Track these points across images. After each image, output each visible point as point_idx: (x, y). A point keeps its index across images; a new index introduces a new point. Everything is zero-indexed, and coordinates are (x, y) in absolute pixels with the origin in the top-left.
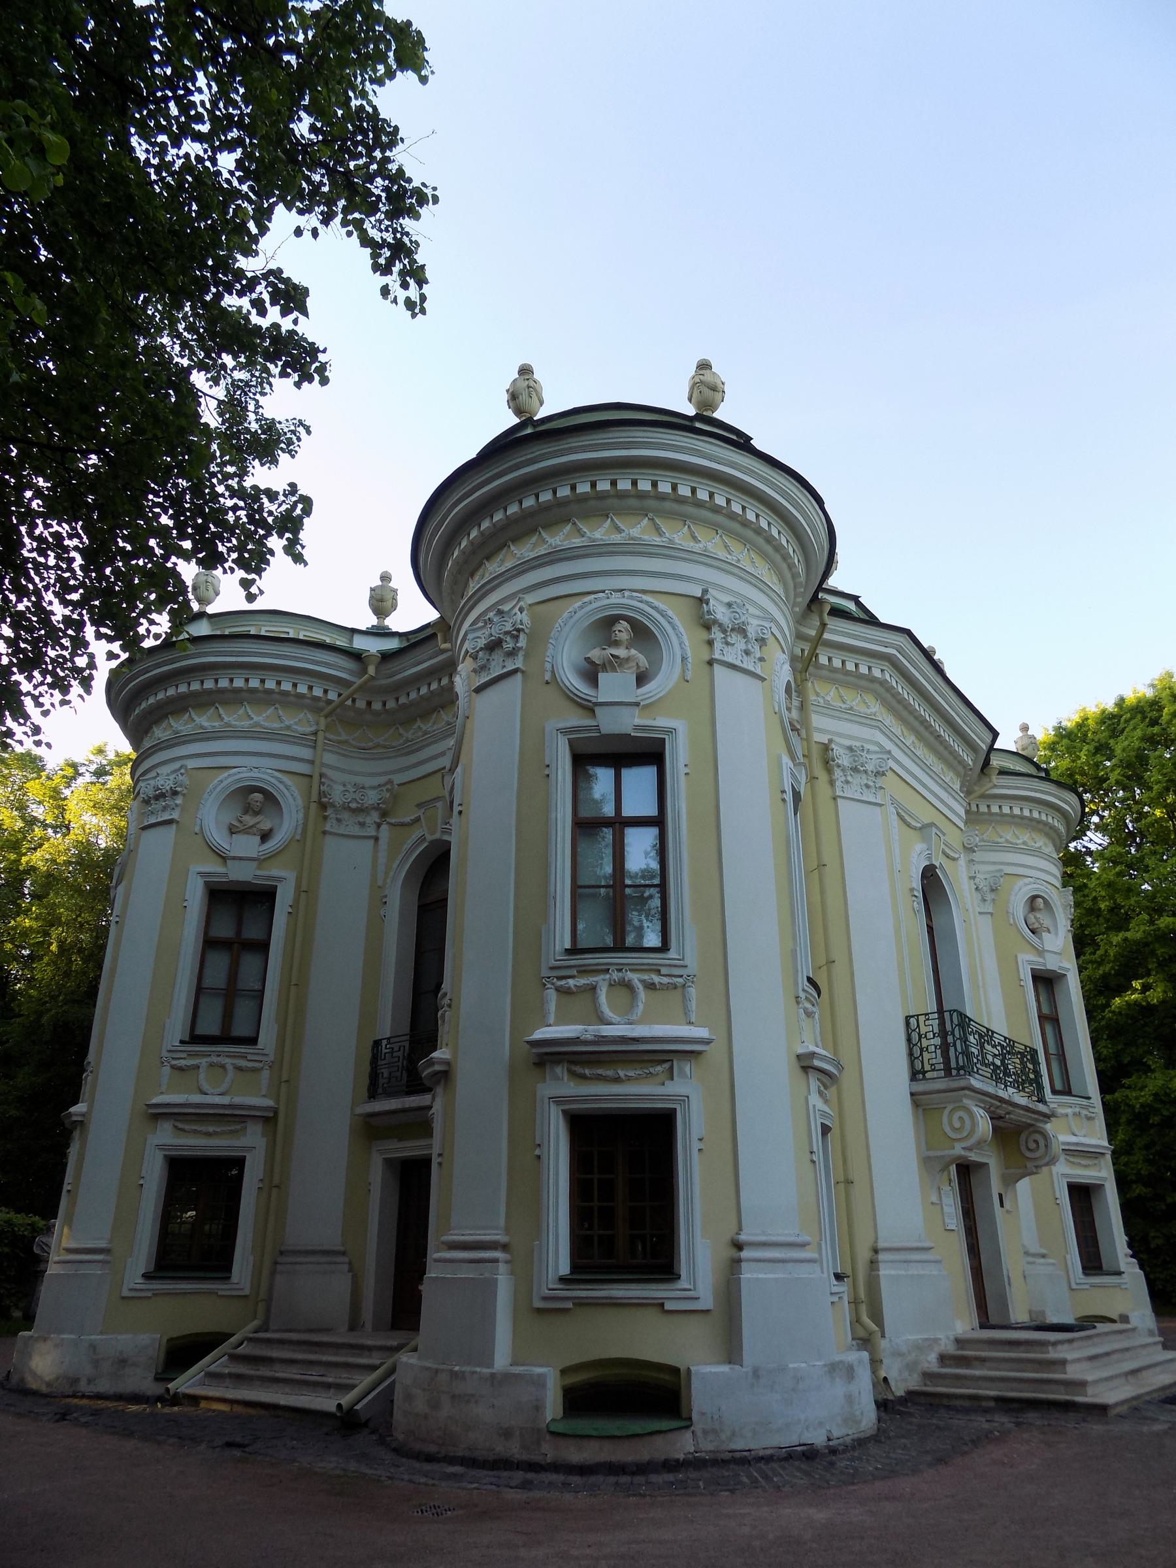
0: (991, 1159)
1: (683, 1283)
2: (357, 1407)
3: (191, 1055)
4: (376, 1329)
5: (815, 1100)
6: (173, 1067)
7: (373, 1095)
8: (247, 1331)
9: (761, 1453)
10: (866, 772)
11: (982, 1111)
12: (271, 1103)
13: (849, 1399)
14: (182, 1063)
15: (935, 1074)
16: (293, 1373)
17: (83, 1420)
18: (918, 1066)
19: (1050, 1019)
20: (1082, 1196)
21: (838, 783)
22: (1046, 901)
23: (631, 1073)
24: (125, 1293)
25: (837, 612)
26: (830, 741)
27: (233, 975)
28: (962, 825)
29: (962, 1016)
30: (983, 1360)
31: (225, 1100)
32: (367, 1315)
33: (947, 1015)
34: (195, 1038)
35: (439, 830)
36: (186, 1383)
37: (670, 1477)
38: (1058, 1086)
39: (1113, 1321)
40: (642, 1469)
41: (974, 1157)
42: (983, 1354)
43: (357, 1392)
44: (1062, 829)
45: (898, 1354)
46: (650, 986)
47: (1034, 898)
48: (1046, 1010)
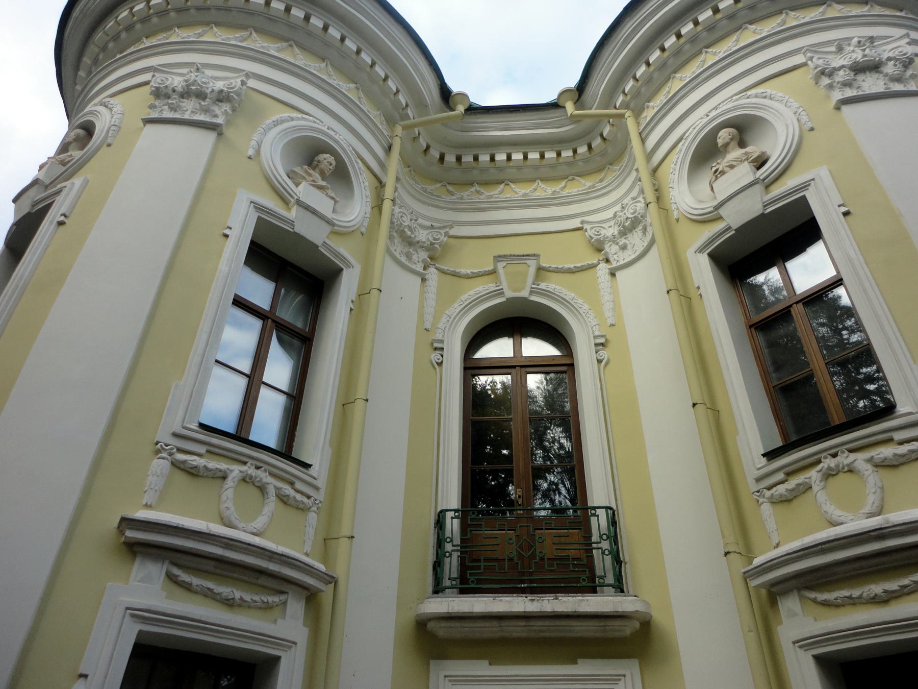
6: (175, 464)
23: (247, 598)
35: (528, 289)
46: (283, 499)
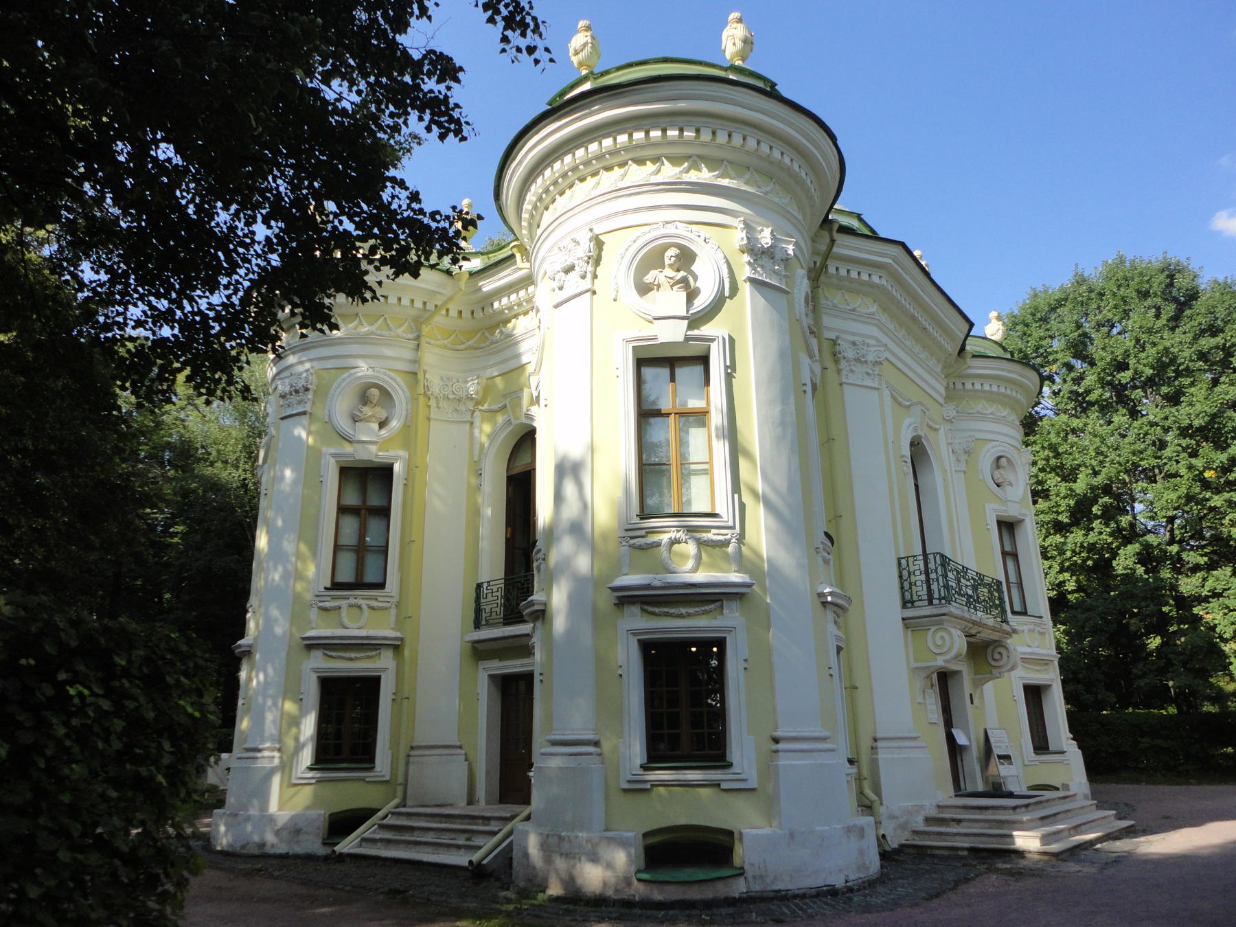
0: (963, 667)
1: (735, 769)
2: (485, 862)
3: (334, 598)
4: (488, 803)
5: (831, 628)
7: (477, 625)
8: (390, 806)
9: (797, 892)
10: (866, 362)
11: (959, 632)
12: (398, 634)
13: (861, 852)
14: (327, 604)
15: (920, 603)
16: (429, 837)
17: (277, 873)
18: (907, 596)
19: (1010, 555)
20: (1034, 694)
21: (844, 373)
22: (1008, 460)
24: (294, 781)
25: (845, 230)
26: (837, 338)
27: (362, 533)
28: (942, 401)
29: (942, 556)
30: (959, 821)
31: (363, 633)
32: (481, 793)
33: (931, 557)
34: (336, 586)
36: (347, 845)
37: (731, 910)
38: (1017, 608)
39: (1057, 789)
40: (709, 904)
41: (954, 667)
42: (959, 817)
43: (484, 850)
44: (1023, 400)
45: (892, 817)
47: (999, 458)
48: (1008, 548)
